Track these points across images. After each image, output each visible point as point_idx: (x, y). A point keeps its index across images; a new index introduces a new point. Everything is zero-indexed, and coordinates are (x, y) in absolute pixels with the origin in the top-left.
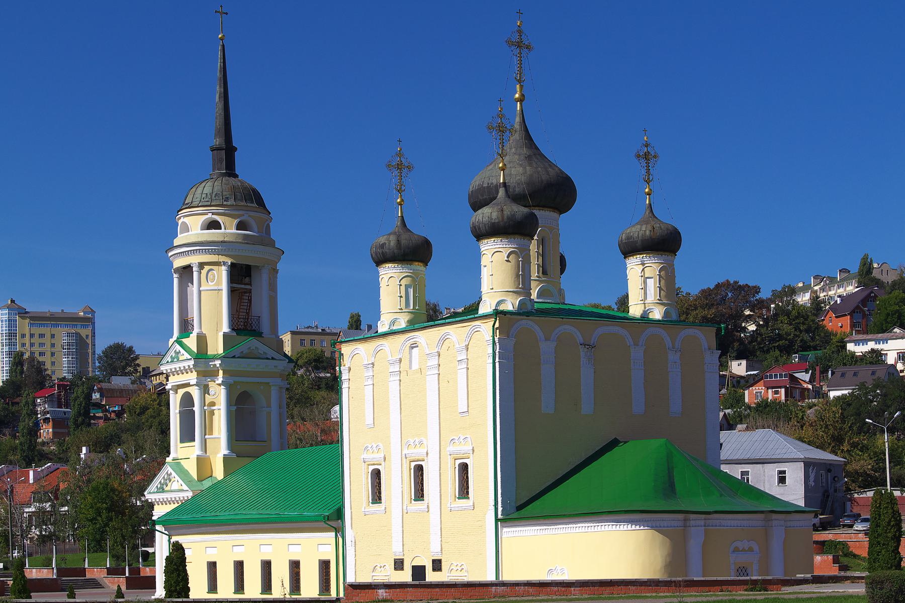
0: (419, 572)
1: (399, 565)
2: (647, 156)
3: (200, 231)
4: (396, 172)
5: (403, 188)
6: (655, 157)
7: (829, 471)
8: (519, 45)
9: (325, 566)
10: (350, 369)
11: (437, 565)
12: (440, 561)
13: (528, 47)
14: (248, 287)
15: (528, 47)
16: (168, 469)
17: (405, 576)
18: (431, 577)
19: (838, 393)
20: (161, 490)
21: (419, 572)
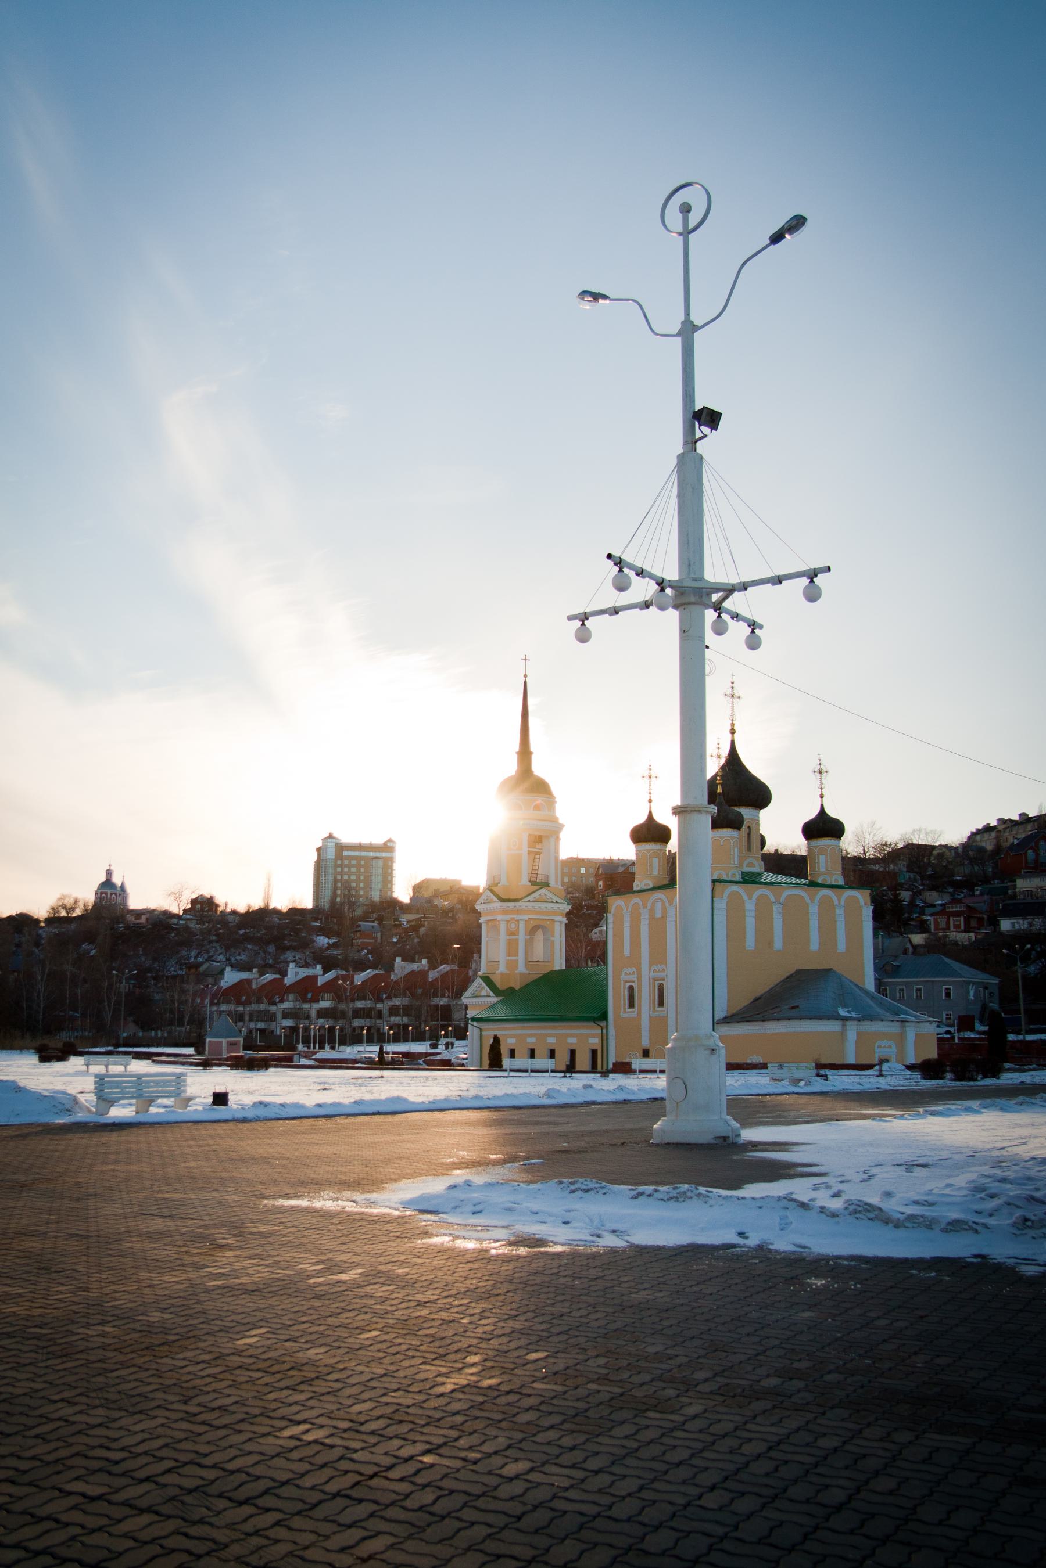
7: (986, 988)
9: (594, 1053)
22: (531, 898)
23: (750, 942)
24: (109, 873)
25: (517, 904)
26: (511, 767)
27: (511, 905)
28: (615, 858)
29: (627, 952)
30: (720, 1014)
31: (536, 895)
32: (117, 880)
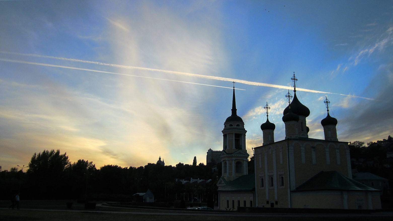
0: (272, 205)
1: (268, 202)
2: (327, 102)
3: (236, 126)
4: (266, 109)
5: (268, 113)
6: (329, 102)
8: (294, 79)
9: (251, 202)
10: (18, 166)
11: (277, 203)
12: (277, 202)
13: (297, 80)
14: (236, 138)
15: (297, 80)
16: (221, 179)
17: (269, 206)
18: (275, 206)
19: (216, 202)
20: (220, 184)
21: (272, 205)
22: (236, 153)
23: (281, 162)
24: (160, 159)
25: (232, 155)
26: (230, 114)
27: (230, 155)
28: (324, 137)
29: (281, 162)
30: (293, 188)
31: (238, 152)
32: (162, 160)
